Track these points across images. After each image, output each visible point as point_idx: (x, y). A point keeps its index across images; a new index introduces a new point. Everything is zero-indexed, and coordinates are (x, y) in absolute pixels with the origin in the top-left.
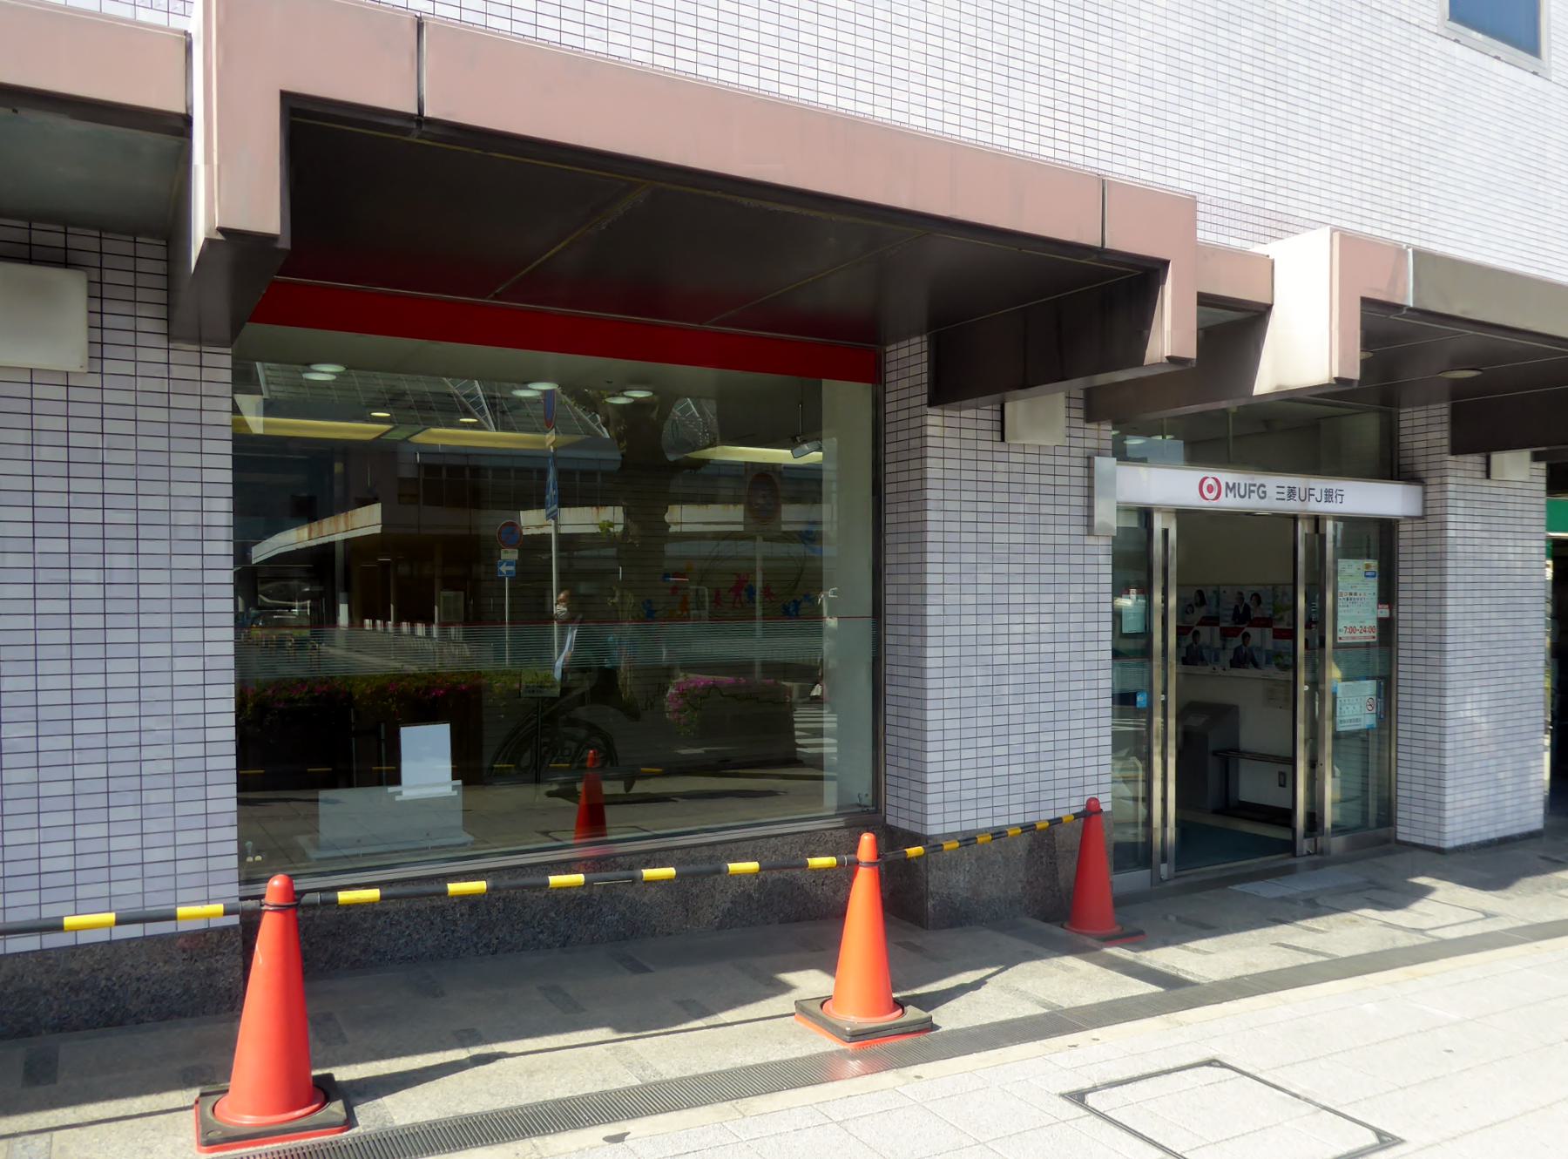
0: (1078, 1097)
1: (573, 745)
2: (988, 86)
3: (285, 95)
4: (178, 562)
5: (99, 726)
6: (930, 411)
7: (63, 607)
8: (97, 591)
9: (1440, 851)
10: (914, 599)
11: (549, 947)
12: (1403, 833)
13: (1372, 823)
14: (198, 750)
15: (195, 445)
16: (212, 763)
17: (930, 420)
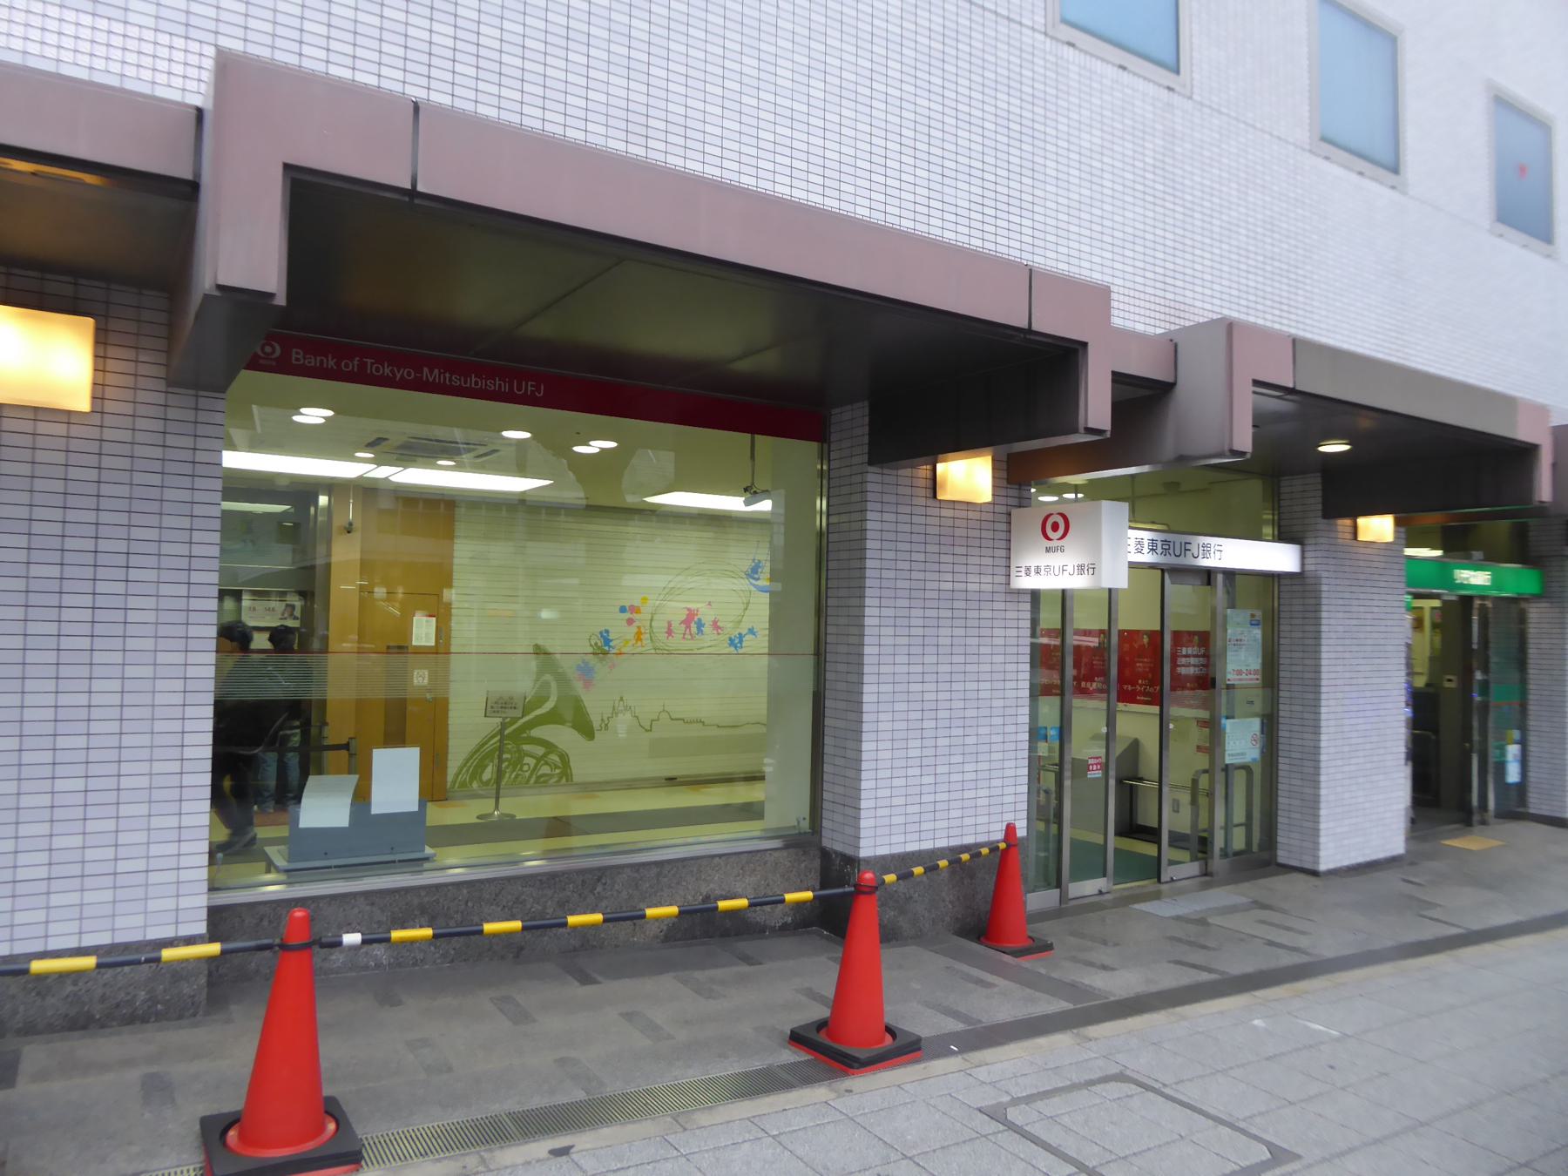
0: (996, 1114)
1: (532, 762)
2: (925, 183)
3: (287, 166)
4: (165, 589)
5: (81, 742)
6: (871, 469)
7: (52, 628)
8: (86, 615)
9: (1315, 873)
10: (852, 640)
11: (503, 958)
12: (1283, 856)
13: (1255, 848)
14: (175, 767)
15: (187, 482)
16: (188, 780)
17: (870, 477)
